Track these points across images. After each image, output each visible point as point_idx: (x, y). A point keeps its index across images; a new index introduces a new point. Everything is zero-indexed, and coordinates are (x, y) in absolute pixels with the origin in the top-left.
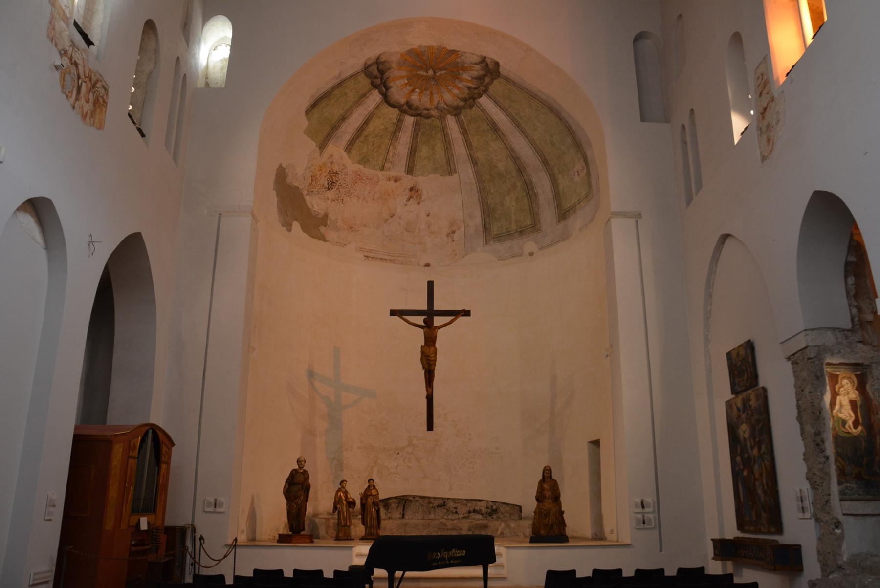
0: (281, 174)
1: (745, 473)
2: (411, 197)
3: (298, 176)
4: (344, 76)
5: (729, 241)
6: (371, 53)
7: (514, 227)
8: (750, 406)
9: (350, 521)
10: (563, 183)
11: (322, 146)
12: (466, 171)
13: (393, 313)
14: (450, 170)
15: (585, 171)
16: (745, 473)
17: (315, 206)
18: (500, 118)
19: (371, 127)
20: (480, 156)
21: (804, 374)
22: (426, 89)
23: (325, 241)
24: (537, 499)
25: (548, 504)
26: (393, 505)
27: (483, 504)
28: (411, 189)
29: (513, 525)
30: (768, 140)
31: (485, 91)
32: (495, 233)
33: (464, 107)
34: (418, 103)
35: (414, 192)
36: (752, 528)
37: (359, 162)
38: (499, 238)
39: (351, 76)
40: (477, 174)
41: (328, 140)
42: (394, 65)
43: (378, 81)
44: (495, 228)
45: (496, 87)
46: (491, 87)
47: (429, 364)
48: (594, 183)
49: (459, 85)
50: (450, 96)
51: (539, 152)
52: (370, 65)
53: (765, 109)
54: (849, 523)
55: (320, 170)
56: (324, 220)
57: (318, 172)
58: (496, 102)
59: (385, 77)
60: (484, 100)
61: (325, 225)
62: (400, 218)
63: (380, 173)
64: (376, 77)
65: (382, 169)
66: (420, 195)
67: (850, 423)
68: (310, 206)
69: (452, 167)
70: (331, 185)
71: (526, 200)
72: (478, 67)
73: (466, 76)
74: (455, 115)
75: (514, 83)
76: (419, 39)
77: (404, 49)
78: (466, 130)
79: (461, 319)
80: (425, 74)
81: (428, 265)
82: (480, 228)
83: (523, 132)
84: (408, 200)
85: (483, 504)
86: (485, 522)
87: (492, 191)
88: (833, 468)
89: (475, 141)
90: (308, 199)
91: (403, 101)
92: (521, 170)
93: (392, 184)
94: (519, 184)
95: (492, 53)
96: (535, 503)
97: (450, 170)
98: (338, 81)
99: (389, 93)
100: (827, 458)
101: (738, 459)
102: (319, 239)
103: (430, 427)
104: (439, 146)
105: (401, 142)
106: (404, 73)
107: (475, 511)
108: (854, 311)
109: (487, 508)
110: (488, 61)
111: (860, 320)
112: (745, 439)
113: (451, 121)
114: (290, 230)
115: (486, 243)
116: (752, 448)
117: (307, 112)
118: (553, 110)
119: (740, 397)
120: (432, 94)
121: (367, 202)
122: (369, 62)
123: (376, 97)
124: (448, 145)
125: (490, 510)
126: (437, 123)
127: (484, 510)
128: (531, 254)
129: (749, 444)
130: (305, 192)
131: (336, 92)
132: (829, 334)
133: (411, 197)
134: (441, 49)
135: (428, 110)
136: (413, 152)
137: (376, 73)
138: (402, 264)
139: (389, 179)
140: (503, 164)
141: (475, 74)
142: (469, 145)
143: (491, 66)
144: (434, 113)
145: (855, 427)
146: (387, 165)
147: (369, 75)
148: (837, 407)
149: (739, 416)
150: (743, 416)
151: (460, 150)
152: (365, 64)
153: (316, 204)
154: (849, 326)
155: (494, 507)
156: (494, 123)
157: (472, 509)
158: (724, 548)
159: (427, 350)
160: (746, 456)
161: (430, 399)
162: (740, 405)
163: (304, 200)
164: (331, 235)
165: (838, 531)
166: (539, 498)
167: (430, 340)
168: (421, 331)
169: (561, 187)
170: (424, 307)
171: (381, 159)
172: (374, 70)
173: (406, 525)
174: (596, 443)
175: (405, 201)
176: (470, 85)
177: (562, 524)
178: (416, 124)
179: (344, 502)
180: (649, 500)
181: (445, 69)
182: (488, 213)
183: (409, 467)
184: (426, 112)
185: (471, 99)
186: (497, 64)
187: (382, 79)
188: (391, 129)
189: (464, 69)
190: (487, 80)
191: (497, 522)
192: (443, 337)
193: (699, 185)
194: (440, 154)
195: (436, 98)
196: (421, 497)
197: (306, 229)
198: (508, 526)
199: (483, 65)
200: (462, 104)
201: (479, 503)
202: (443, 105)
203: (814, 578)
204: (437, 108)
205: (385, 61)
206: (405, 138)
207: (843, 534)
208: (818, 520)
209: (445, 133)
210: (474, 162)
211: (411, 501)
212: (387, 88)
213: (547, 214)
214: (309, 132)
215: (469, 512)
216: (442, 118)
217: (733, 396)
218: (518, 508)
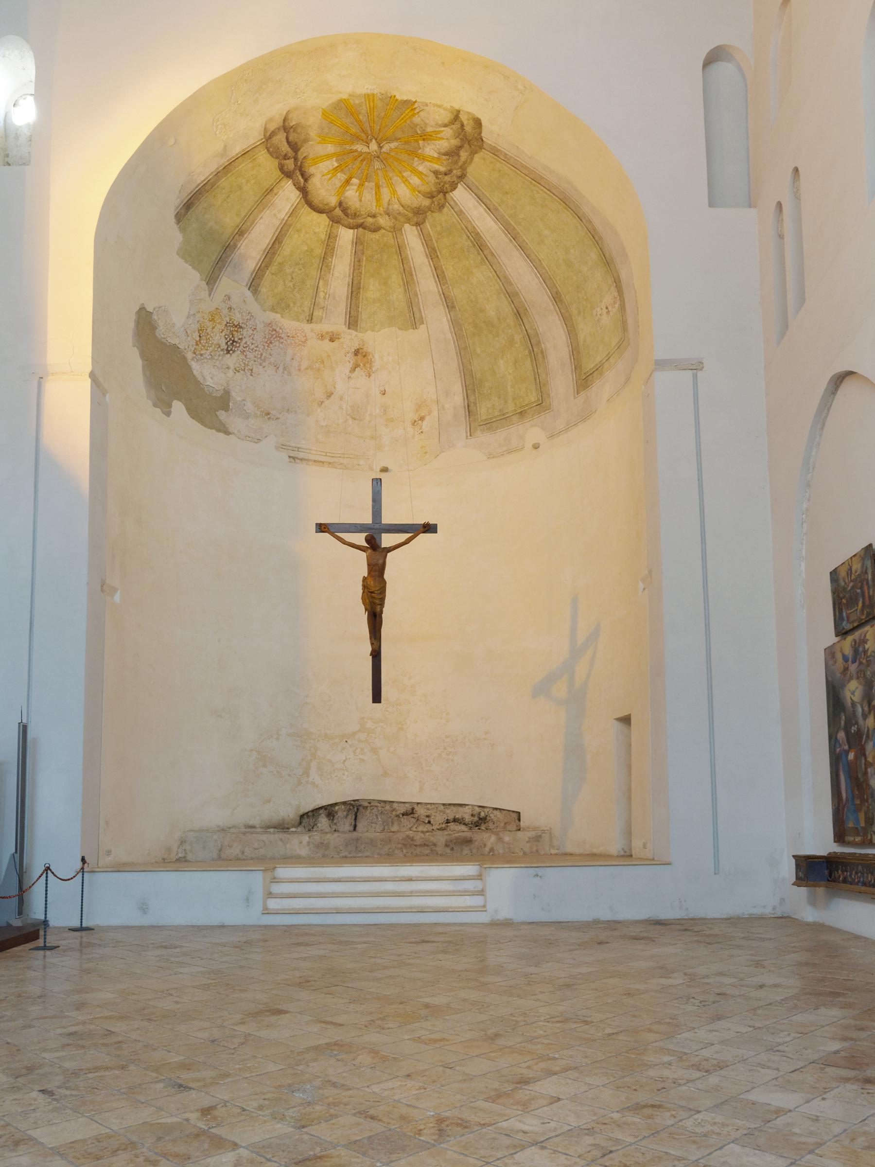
0: (145, 322)
1: (851, 756)
2: (356, 366)
3: (177, 323)
5: (848, 387)
6: (271, 109)
7: (511, 407)
8: (865, 652)
10: (585, 330)
11: (212, 280)
14: (413, 318)
16: (851, 756)
17: (208, 378)
19: (286, 249)
20: (457, 293)
22: (367, 178)
23: (227, 433)
26: (340, 814)
28: (356, 353)
29: (507, 839)
31: (462, 177)
32: (484, 417)
33: (429, 209)
34: (357, 205)
36: (858, 839)
38: (490, 425)
40: (455, 324)
41: (220, 270)
42: (313, 134)
43: (290, 164)
44: (483, 411)
45: (479, 167)
46: (471, 170)
50: (406, 190)
51: (547, 280)
52: (273, 134)
55: (212, 320)
56: (224, 401)
57: (210, 324)
59: (300, 156)
60: (460, 195)
61: (226, 409)
62: (341, 398)
63: (307, 327)
64: (286, 157)
65: (310, 320)
66: (371, 362)
68: (200, 378)
69: (417, 315)
70: (231, 346)
71: (528, 362)
72: (448, 132)
73: (430, 150)
74: (418, 224)
75: (507, 159)
77: (326, 101)
78: (434, 249)
79: (423, 537)
80: (365, 149)
82: (462, 412)
83: (522, 247)
84: (353, 370)
85: (467, 810)
86: (468, 834)
87: (478, 350)
90: (195, 366)
91: (333, 201)
92: (520, 314)
93: (326, 345)
97: (413, 318)
98: (224, 161)
99: (310, 187)
101: (841, 735)
102: (219, 431)
103: (377, 697)
104: (396, 279)
105: (336, 274)
106: (330, 148)
107: (455, 820)
109: (472, 815)
110: (463, 117)
112: (853, 704)
113: (411, 235)
114: (168, 414)
116: (865, 716)
117: (179, 217)
118: (568, 202)
119: (850, 638)
120: (378, 187)
121: (290, 374)
122: (272, 127)
123: (288, 195)
125: (476, 819)
126: (389, 238)
127: (468, 818)
128: (536, 447)
129: (859, 710)
130: (189, 355)
131: (223, 183)
133: (356, 366)
134: (390, 100)
135: (374, 216)
136: (355, 290)
137: (285, 148)
139: (322, 337)
140: (495, 306)
142: (440, 276)
144: (383, 221)
147: (274, 153)
149: (846, 669)
150: (853, 668)
151: (427, 284)
152: (266, 130)
153: (210, 374)
155: (483, 815)
156: (477, 234)
157: (451, 817)
158: (815, 871)
160: (854, 729)
161: (376, 655)
162: (848, 651)
163: (189, 367)
167: (377, 570)
168: (363, 556)
169: (581, 337)
170: (368, 519)
171: (307, 303)
172: (280, 139)
173: (357, 840)
174: (626, 720)
175: (347, 372)
176: (437, 167)
178: (358, 242)
181: (397, 139)
182: (472, 387)
183: (363, 760)
184: (370, 220)
185: (440, 194)
186: (478, 123)
187: (296, 159)
188: (319, 251)
189: (426, 137)
190: (464, 155)
191: (485, 835)
192: (394, 563)
193: (802, 299)
194: (398, 295)
196: (380, 802)
197: (195, 413)
198: (500, 839)
199: (457, 126)
200: (426, 202)
201: (461, 809)
202: (396, 207)
205: (298, 125)
206: (342, 266)
209: (400, 249)
210: (450, 304)
213: (561, 382)
215: (448, 822)
216: (396, 230)
217: (836, 639)
218: (515, 816)
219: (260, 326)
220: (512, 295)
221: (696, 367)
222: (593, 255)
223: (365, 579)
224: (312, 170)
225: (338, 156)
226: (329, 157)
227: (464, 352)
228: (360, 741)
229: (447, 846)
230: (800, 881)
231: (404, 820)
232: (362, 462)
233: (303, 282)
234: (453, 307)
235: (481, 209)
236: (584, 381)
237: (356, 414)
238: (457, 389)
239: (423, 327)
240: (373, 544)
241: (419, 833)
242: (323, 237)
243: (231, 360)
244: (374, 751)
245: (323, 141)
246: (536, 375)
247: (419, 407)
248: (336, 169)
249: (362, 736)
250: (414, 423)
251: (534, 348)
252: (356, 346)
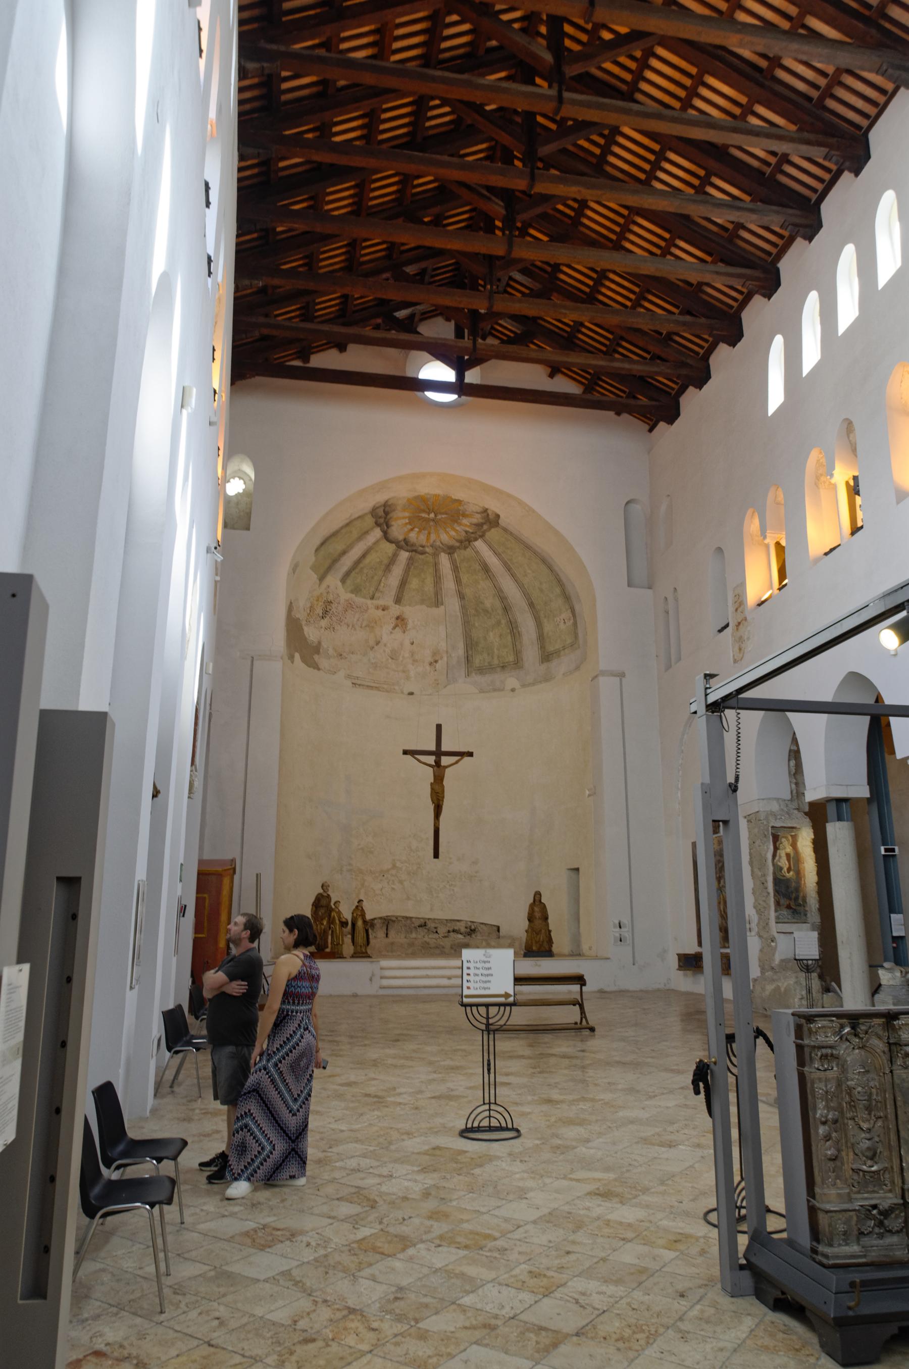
4: (353, 517)
6: (380, 498)
7: (496, 661)
9: (343, 940)
10: (548, 627)
11: (321, 579)
12: (452, 604)
13: (405, 752)
14: (437, 601)
15: (572, 621)
18: (493, 561)
19: (367, 561)
20: (468, 592)
21: (756, 830)
22: (424, 529)
23: (319, 669)
24: (529, 920)
25: (538, 923)
26: (378, 925)
27: (463, 924)
28: (397, 618)
30: (740, 649)
33: (458, 547)
35: (400, 621)
37: (352, 592)
38: (481, 671)
39: (359, 517)
40: (463, 607)
43: (382, 520)
44: (477, 661)
47: (438, 800)
48: (580, 635)
49: (458, 528)
50: (446, 537)
53: (739, 623)
54: (781, 938)
55: (317, 600)
58: (491, 547)
60: (479, 544)
61: (318, 652)
62: (385, 645)
63: (369, 602)
64: (380, 517)
65: (372, 598)
66: (406, 624)
67: (785, 869)
69: (440, 600)
71: (509, 637)
72: (479, 516)
73: (465, 521)
74: (449, 554)
75: (511, 534)
76: (426, 488)
80: (426, 516)
81: (411, 694)
83: (513, 575)
84: (394, 628)
87: (477, 624)
88: (772, 900)
89: (465, 578)
90: (305, 629)
91: (401, 538)
92: (507, 609)
94: (503, 622)
95: (494, 506)
96: (527, 922)
97: (437, 601)
98: (347, 521)
99: (389, 531)
100: (769, 893)
102: (314, 668)
104: (429, 580)
106: (407, 514)
107: (454, 931)
108: (794, 786)
111: (797, 792)
113: (444, 559)
115: (468, 674)
120: (429, 533)
123: (377, 533)
124: (438, 579)
126: (430, 559)
127: (463, 930)
130: (304, 623)
131: (344, 531)
132: (775, 803)
135: (423, 547)
136: (403, 583)
138: (387, 691)
139: (377, 608)
140: (490, 601)
141: (475, 521)
142: (458, 581)
143: (491, 517)
145: (788, 872)
146: (377, 595)
148: (777, 858)
151: (449, 584)
153: (311, 633)
154: (789, 797)
155: (473, 927)
159: (436, 787)
164: (323, 663)
165: (773, 944)
166: (531, 919)
167: (439, 779)
170: (433, 747)
171: (372, 589)
172: (381, 512)
176: (468, 529)
177: (550, 941)
178: (410, 559)
179: (337, 922)
180: (626, 921)
182: (471, 645)
183: (393, 889)
185: (467, 541)
186: (498, 516)
188: (386, 561)
189: (465, 515)
190: (485, 527)
194: (429, 587)
195: (433, 537)
196: (403, 917)
197: (304, 660)
199: (485, 514)
200: (457, 544)
201: (458, 923)
202: (438, 543)
203: (755, 977)
204: (432, 546)
206: (397, 571)
207: (776, 946)
208: (760, 937)
209: (436, 565)
210: (462, 596)
211: (394, 921)
212: (388, 526)
213: (530, 654)
214: (314, 568)
215: (449, 932)
216: (435, 555)
218: (496, 929)
219: (342, 601)
220: (503, 599)
221: (622, 675)
222: (558, 590)
223: (431, 784)
224: (393, 523)
225: (409, 518)
226: (404, 518)
227: (467, 624)
228: (392, 875)
229: (452, 948)
230: (680, 968)
231: (420, 930)
232: (397, 688)
233: (373, 577)
234: (464, 598)
235: (491, 553)
236: (546, 657)
237: (394, 656)
238: (461, 646)
239: (442, 607)
240: (438, 763)
241: (431, 938)
242: (390, 555)
243: (324, 623)
244: (401, 882)
245: (404, 510)
246: (514, 645)
247: (434, 654)
248: (407, 524)
249: (394, 872)
250: (431, 664)
251: (514, 629)
252: (398, 614)
